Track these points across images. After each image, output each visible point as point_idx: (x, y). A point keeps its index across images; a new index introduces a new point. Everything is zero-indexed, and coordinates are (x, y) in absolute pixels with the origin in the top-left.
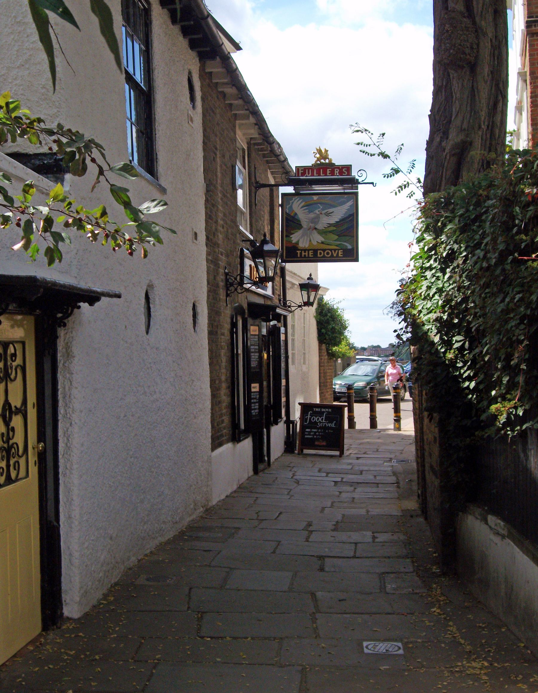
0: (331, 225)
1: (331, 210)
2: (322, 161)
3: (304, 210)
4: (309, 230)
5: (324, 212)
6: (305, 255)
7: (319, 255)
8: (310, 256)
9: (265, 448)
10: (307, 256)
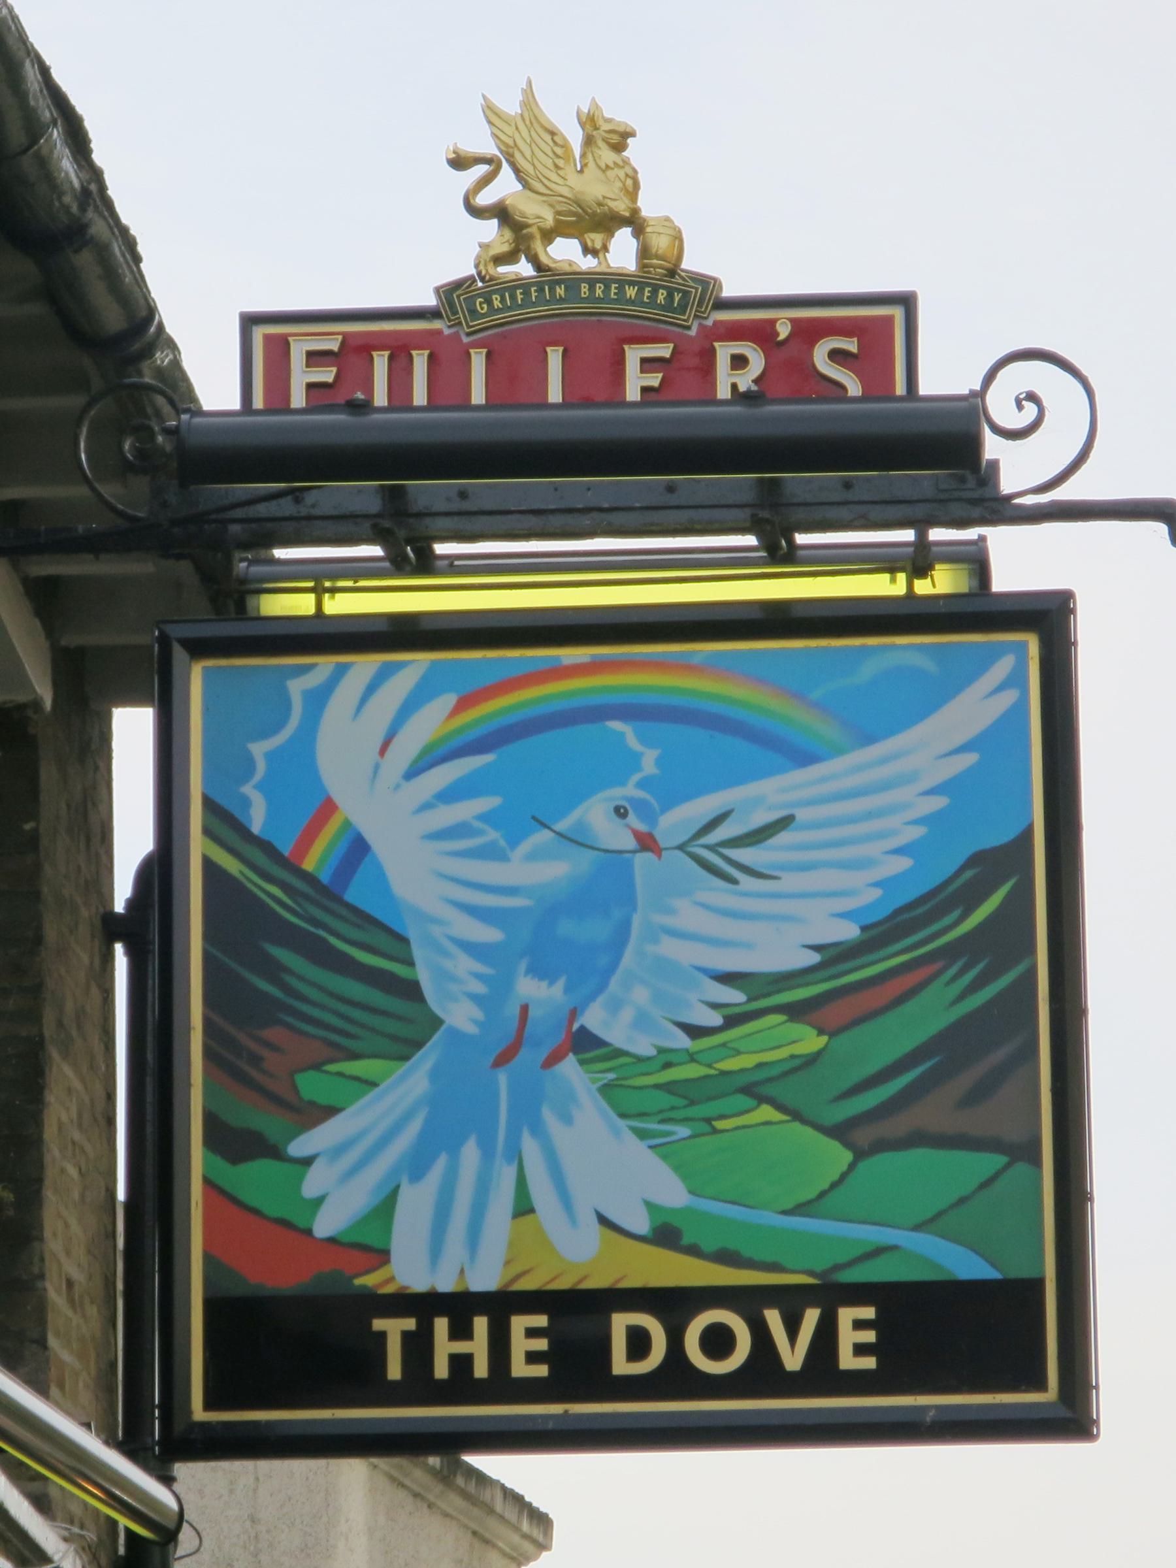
3: (449, 796)
4: (504, 1058)
7: (621, 1365)
8: (520, 1369)
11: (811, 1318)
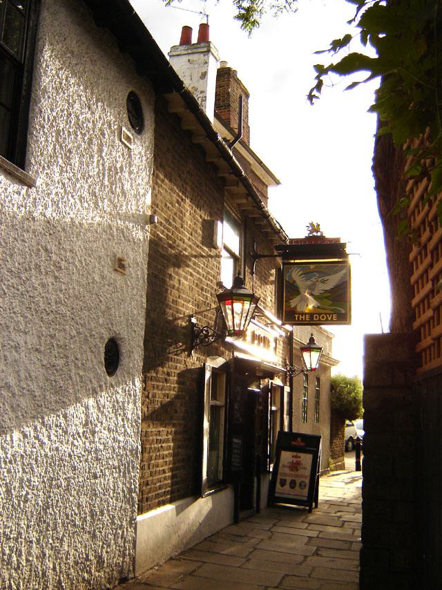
0: (326, 291)
1: (326, 278)
2: (315, 234)
9: (255, 496)
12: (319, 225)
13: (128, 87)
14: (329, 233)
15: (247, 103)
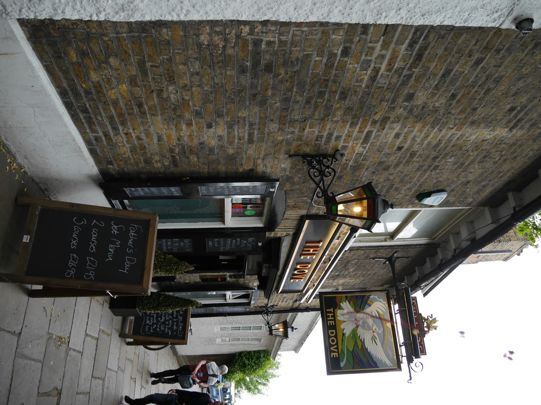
0: (363, 343)
2: (425, 324)
5: (375, 334)
6: (329, 316)
7: (330, 331)
8: (329, 322)
10: (328, 319)
11: (337, 351)
12: (436, 329)
13: (210, 379)
14: (429, 340)
15: (499, 259)
